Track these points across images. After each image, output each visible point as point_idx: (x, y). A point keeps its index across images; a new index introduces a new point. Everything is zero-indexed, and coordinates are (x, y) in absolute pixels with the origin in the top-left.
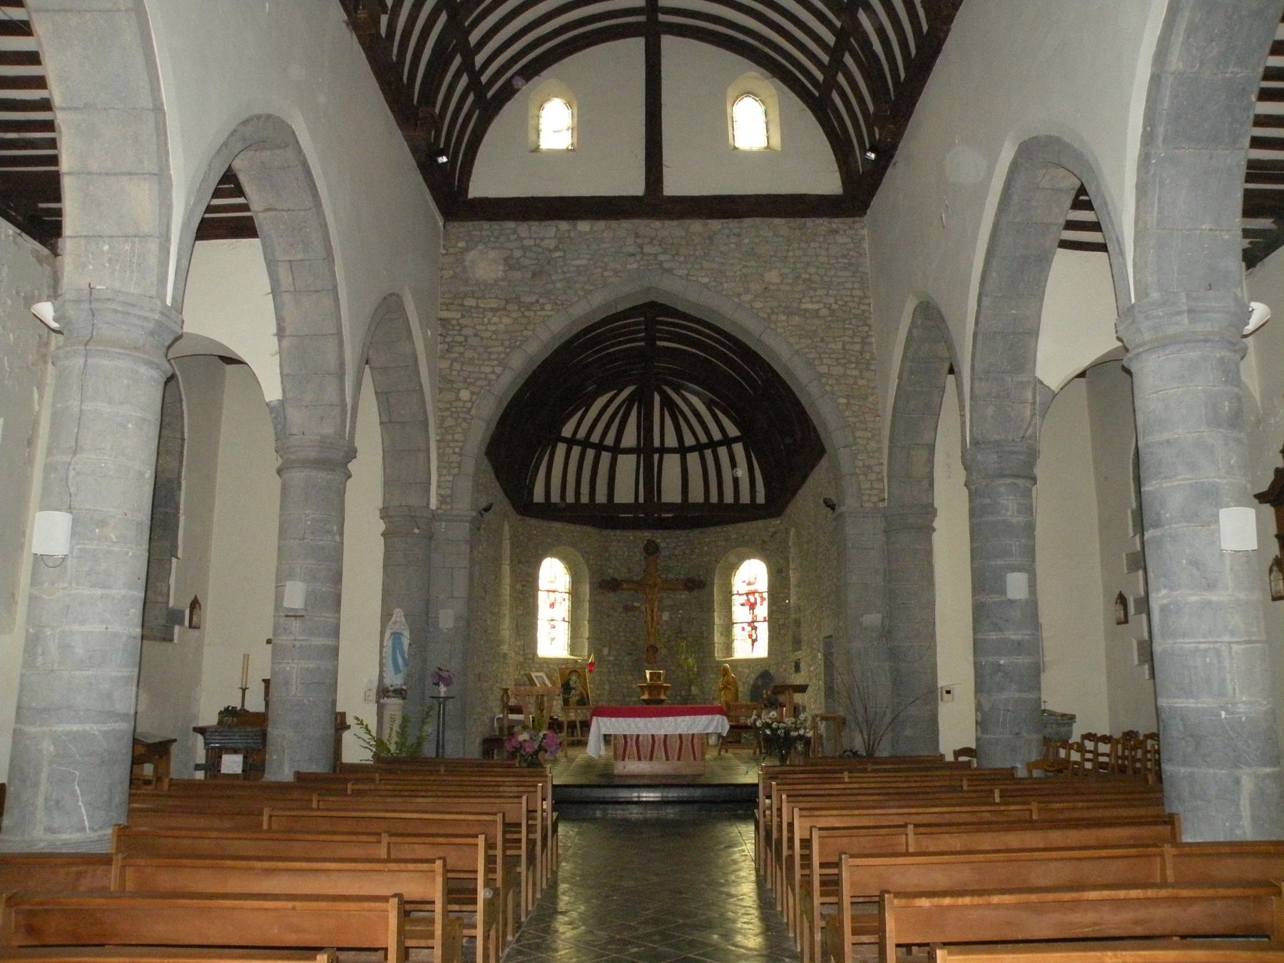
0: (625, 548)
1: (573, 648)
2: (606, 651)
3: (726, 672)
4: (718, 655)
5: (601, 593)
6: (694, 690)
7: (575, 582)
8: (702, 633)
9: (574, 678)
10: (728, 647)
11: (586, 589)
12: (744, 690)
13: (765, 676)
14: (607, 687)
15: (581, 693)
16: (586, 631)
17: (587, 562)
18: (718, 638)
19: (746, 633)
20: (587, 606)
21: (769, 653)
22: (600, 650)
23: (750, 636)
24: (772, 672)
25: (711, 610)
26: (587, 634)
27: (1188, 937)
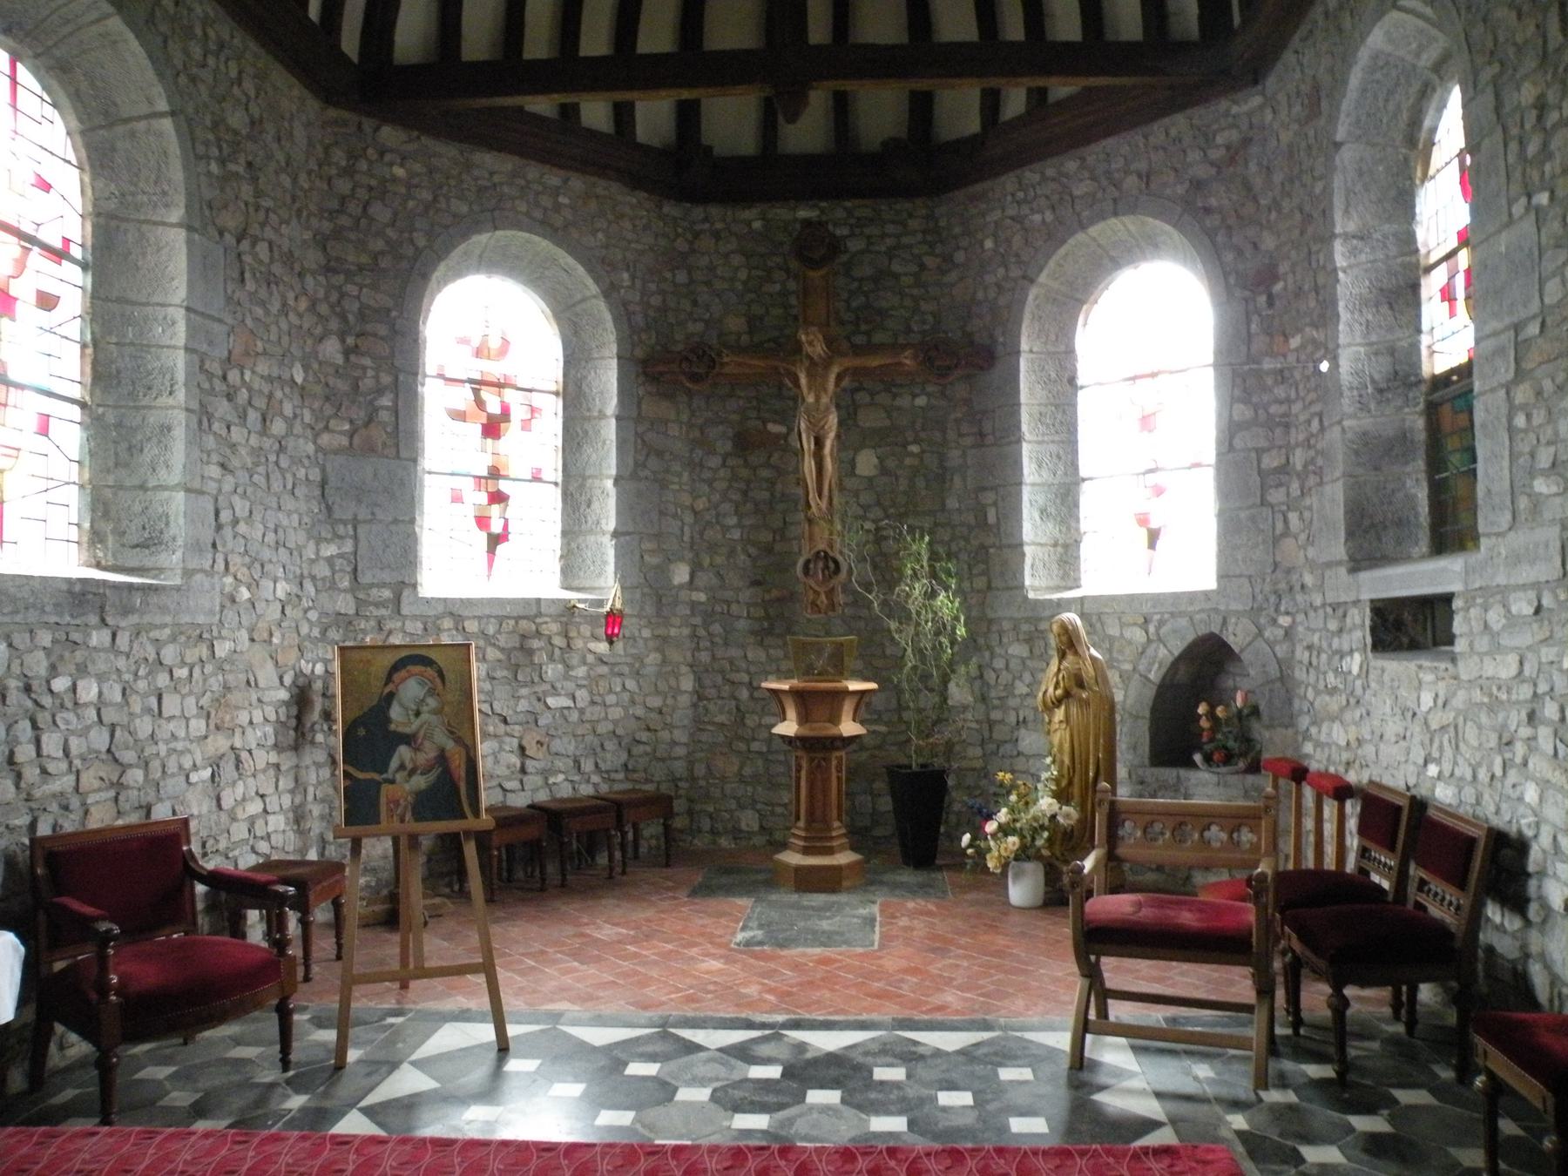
0: (731, 236)
1: (571, 566)
2: (681, 574)
3: (1069, 642)
4: (1036, 581)
5: (688, 388)
6: (959, 693)
7: (576, 359)
8: (981, 512)
9: (411, 688)
10: (1067, 556)
11: (607, 379)
12: (1130, 695)
13: (1206, 662)
14: (687, 684)
15: (442, 758)
16: (607, 510)
17: (609, 292)
18: (1033, 529)
19: (467, 513)
20: (610, 430)
21: (1222, 576)
22: (662, 570)
23: (482, 522)
24: (1236, 637)
25: (1010, 435)
26: (611, 524)
27: (1433, 618)
